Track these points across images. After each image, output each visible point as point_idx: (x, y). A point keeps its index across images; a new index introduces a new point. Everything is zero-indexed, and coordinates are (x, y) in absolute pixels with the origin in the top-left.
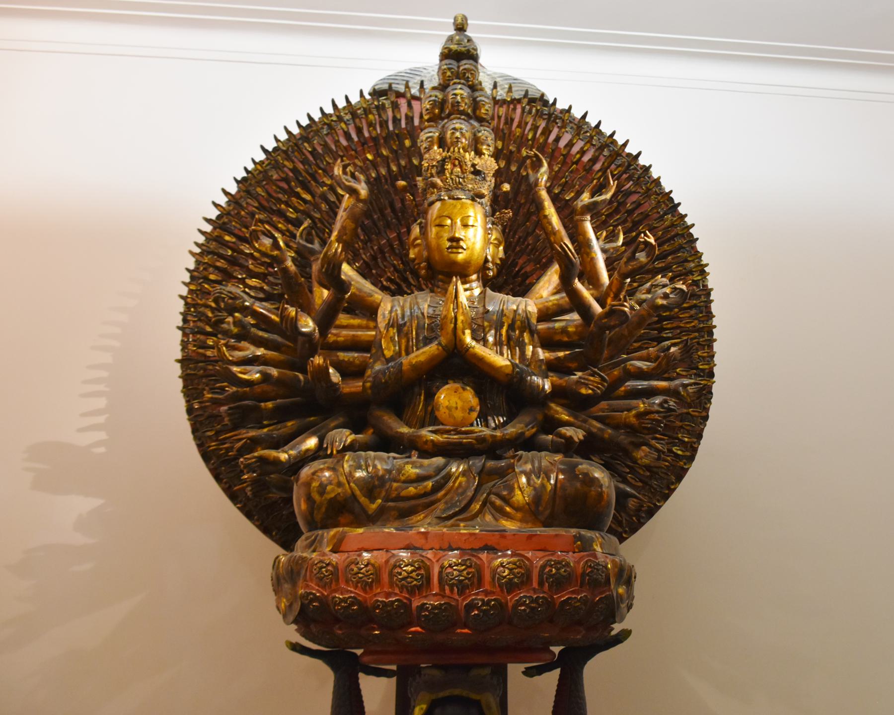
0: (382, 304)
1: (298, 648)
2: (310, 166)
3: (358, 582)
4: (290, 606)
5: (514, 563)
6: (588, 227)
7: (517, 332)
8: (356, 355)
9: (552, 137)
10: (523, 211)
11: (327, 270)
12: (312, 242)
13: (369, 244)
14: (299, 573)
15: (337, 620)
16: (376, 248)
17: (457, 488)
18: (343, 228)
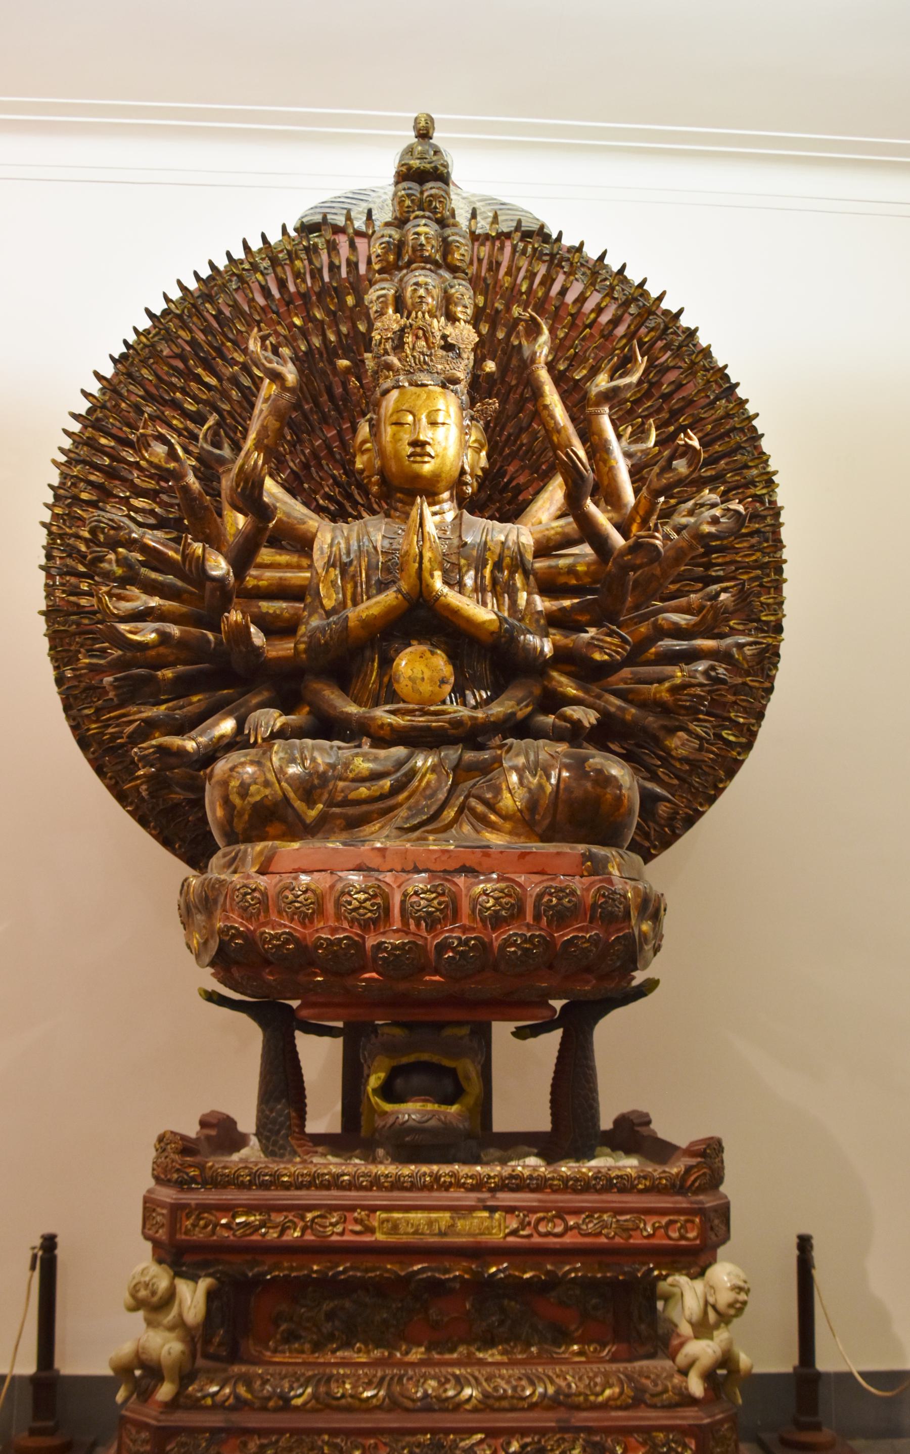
0: (319, 535)
1: (215, 998)
2: (215, 336)
3: (294, 914)
4: (206, 943)
5: (502, 891)
6: (605, 422)
7: (506, 573)
8: (284, 605)
9: (556, 288)
10: (514, 397)
11: (243, 489)
12: (220, 447)
13: (298, 447)
14: (215, 901)
15: (267, 962)
18: (264, 428)
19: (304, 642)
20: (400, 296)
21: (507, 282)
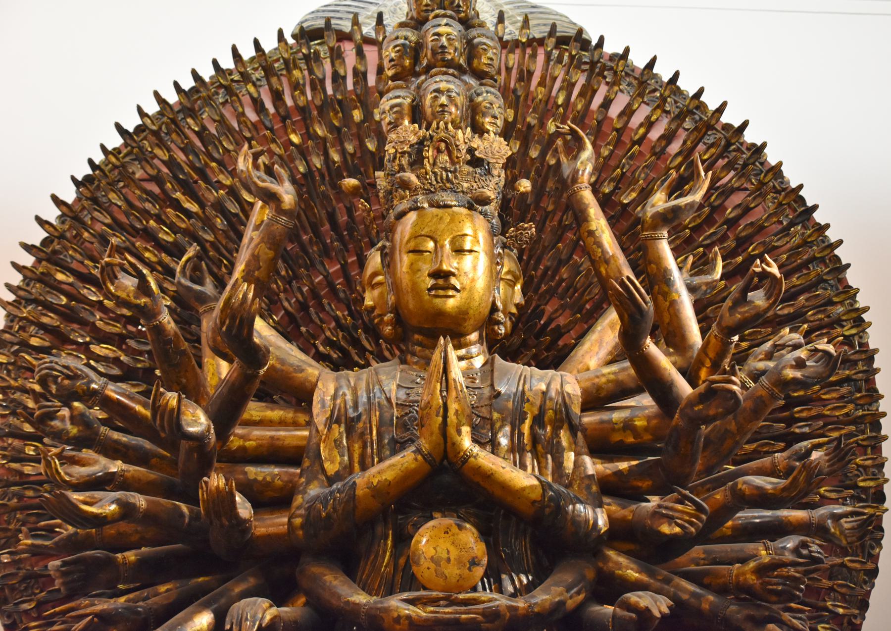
0: (320, 384)
2: (197, 155)
7: (549, 429)
8: (276, 470)
12: (201, 282)
16: (305, 289)
18: (255, 258)
19: (300, 516)
20: (417, 105)
21: (541, 93)
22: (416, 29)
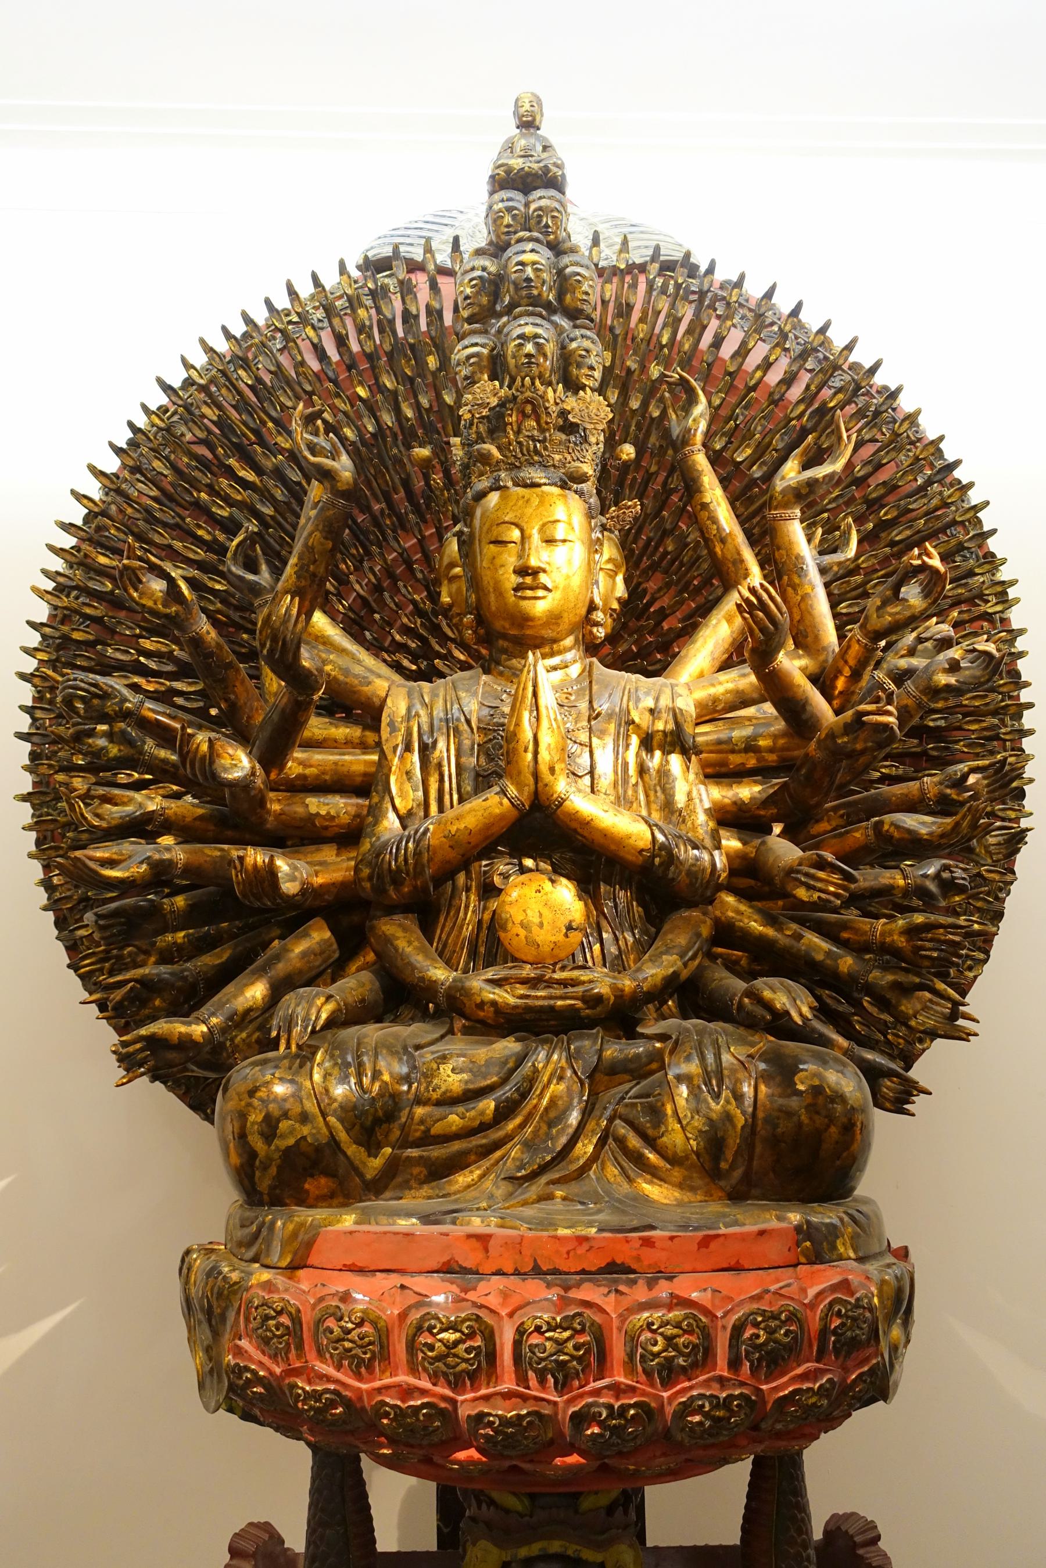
0: (389, 701)
5: (678, 1326)
12: (256, 571)
14: (223, 1318)
16: (377, 568)
17: (546, 1109)
18: (308, 549)
20: (498, 355)
22: (496, 257)
